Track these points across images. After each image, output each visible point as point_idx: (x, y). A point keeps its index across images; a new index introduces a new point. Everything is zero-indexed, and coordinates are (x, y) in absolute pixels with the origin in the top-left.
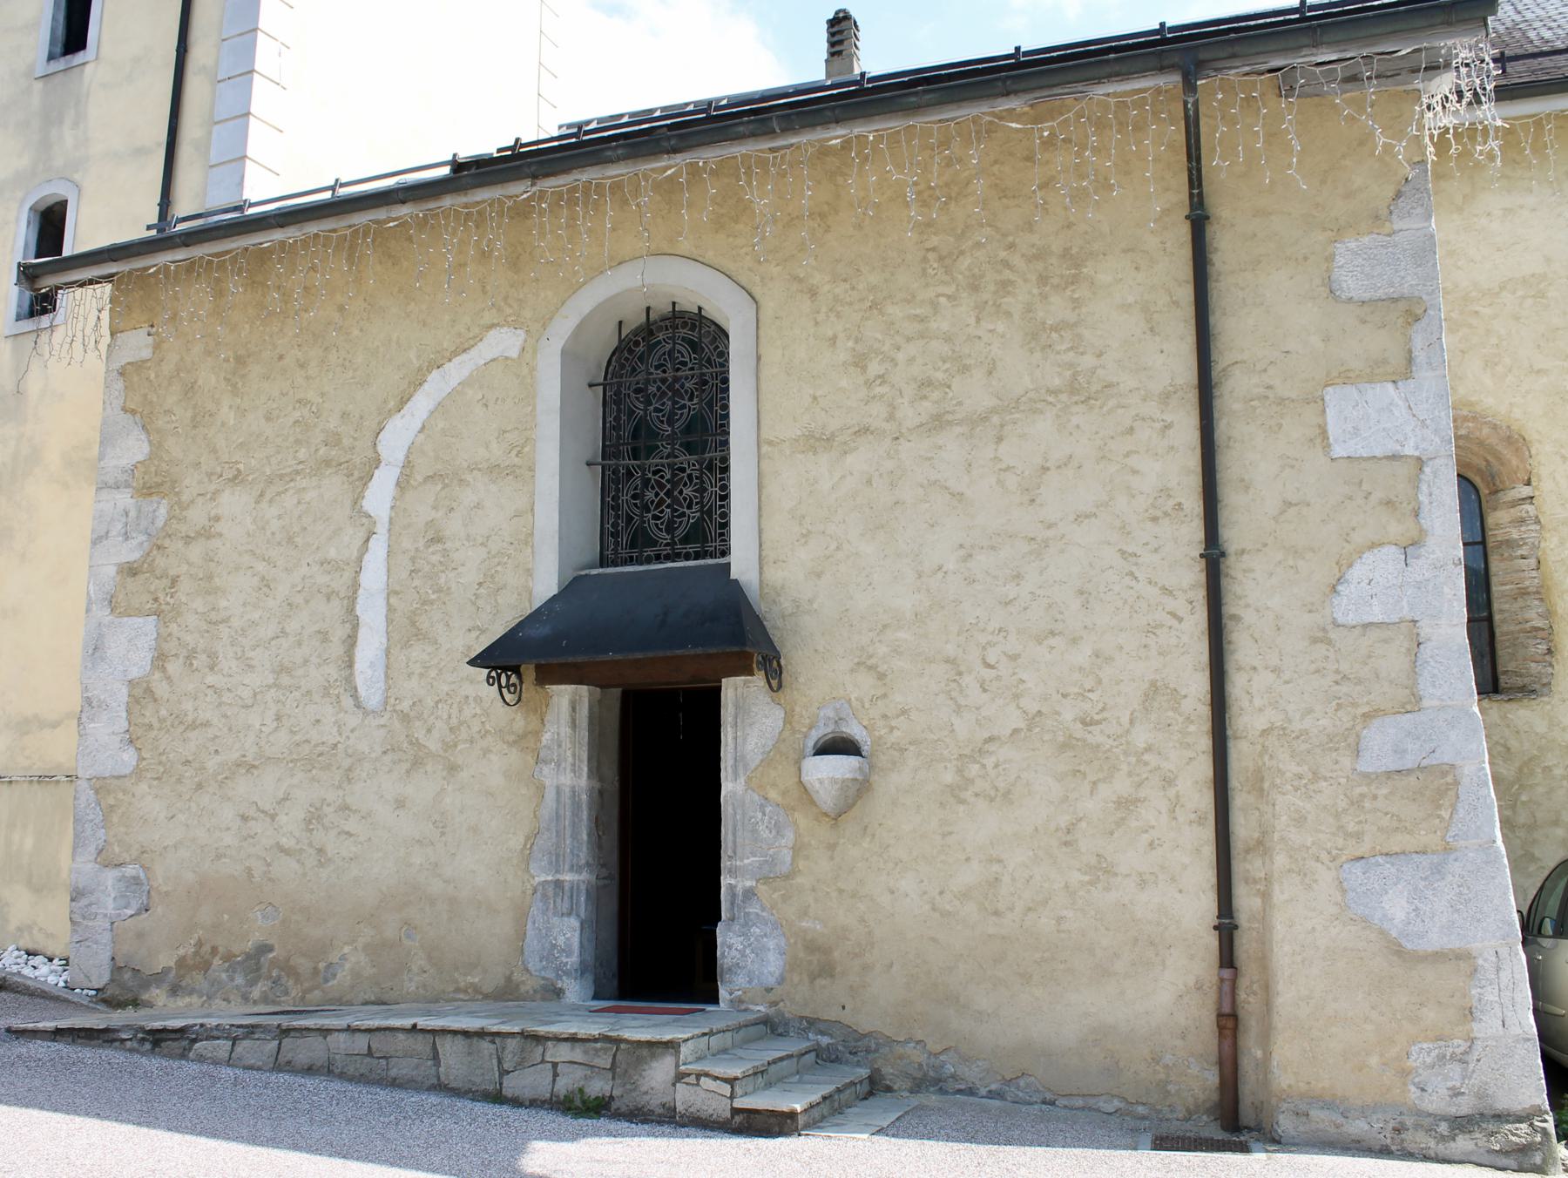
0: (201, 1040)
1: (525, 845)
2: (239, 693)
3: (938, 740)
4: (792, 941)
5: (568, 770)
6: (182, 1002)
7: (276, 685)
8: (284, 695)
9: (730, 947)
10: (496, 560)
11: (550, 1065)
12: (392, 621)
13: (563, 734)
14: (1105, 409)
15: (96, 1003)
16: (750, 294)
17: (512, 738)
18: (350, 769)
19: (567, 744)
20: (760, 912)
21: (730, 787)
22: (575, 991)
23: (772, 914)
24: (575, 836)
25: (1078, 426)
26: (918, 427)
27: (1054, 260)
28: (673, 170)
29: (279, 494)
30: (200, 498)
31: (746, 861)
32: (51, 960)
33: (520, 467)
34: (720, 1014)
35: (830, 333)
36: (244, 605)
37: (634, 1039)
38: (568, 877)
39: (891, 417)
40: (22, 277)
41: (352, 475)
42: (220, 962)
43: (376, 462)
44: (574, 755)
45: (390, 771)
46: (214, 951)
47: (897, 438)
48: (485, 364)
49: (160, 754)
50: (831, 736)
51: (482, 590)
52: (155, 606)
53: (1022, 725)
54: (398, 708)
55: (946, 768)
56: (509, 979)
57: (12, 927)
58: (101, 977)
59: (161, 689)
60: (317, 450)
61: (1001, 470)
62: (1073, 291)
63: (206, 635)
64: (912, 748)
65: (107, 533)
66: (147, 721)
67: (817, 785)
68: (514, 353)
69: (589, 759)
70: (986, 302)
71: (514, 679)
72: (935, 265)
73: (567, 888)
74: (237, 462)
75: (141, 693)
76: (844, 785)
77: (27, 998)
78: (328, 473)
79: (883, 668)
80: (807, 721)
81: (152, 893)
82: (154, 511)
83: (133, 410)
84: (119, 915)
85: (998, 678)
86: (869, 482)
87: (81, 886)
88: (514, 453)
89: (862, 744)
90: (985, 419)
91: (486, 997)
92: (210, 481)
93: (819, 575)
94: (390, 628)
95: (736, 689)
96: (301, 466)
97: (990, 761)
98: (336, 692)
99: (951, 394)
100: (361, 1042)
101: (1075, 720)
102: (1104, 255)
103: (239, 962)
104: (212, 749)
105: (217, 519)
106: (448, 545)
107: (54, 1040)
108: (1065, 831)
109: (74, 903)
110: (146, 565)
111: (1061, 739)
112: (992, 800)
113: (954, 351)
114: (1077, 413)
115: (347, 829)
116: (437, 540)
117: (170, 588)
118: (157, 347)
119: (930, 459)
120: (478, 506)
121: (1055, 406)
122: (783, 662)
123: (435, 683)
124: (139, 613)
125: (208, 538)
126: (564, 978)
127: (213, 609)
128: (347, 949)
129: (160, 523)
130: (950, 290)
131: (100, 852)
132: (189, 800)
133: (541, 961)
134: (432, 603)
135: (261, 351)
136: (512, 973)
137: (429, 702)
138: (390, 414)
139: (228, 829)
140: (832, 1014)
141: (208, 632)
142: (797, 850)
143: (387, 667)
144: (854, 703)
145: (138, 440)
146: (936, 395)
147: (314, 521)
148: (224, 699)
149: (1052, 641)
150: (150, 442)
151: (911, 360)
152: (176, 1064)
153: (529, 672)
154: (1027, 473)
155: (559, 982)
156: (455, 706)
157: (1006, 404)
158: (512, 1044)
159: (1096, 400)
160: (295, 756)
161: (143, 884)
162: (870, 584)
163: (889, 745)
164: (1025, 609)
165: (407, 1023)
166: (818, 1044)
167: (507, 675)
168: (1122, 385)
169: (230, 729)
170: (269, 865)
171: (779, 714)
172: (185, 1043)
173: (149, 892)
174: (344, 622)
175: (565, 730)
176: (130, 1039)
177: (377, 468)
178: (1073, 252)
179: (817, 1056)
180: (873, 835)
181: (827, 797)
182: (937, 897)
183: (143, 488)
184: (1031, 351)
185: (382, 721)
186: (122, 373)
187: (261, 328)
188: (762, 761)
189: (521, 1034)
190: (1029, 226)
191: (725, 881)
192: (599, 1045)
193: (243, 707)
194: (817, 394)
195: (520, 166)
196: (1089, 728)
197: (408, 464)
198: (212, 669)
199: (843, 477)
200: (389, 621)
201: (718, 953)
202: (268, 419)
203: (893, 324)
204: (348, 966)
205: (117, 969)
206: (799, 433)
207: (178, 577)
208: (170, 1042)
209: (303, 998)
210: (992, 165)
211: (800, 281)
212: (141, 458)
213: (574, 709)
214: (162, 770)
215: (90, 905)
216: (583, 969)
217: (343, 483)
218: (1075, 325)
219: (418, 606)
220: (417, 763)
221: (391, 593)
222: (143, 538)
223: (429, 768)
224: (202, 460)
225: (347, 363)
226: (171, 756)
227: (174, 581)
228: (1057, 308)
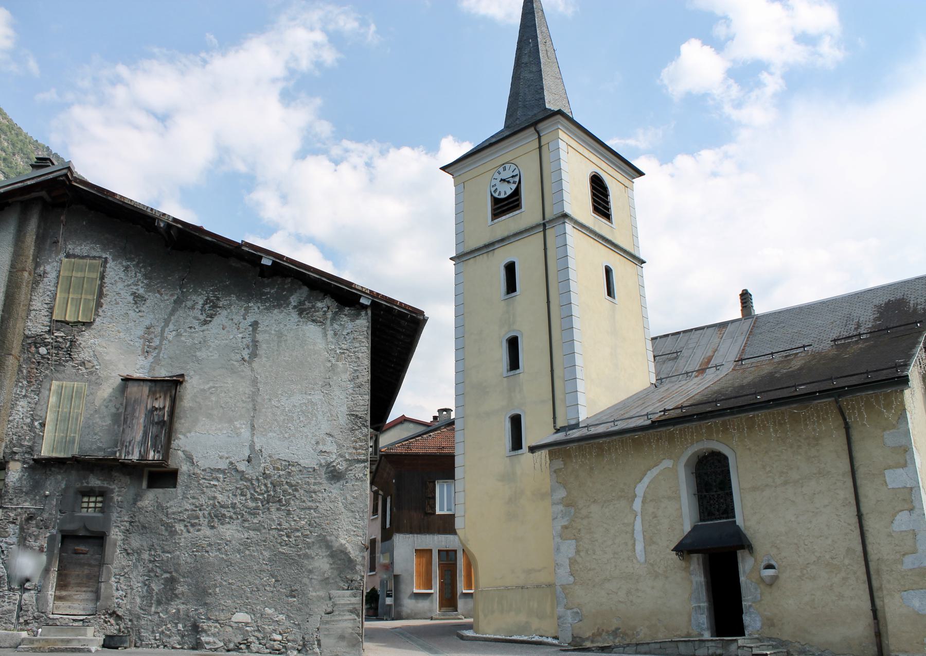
21: (742, 579)
43: (635, 496)
53: (816, 559)
59: (579, 559)
68: (671, 466)
79: (778, 546)
93: (760, 523)
105: (590, 513)
116: (655, 517)
120: (666, 508)
124: (570, 539)
130: (785, 448)
137: (658, 560)
143: (645, 551)
158: (696, 643)
169: (601, 570)
197: (644, 497)
198: (594, 554)
200: (644, 539)
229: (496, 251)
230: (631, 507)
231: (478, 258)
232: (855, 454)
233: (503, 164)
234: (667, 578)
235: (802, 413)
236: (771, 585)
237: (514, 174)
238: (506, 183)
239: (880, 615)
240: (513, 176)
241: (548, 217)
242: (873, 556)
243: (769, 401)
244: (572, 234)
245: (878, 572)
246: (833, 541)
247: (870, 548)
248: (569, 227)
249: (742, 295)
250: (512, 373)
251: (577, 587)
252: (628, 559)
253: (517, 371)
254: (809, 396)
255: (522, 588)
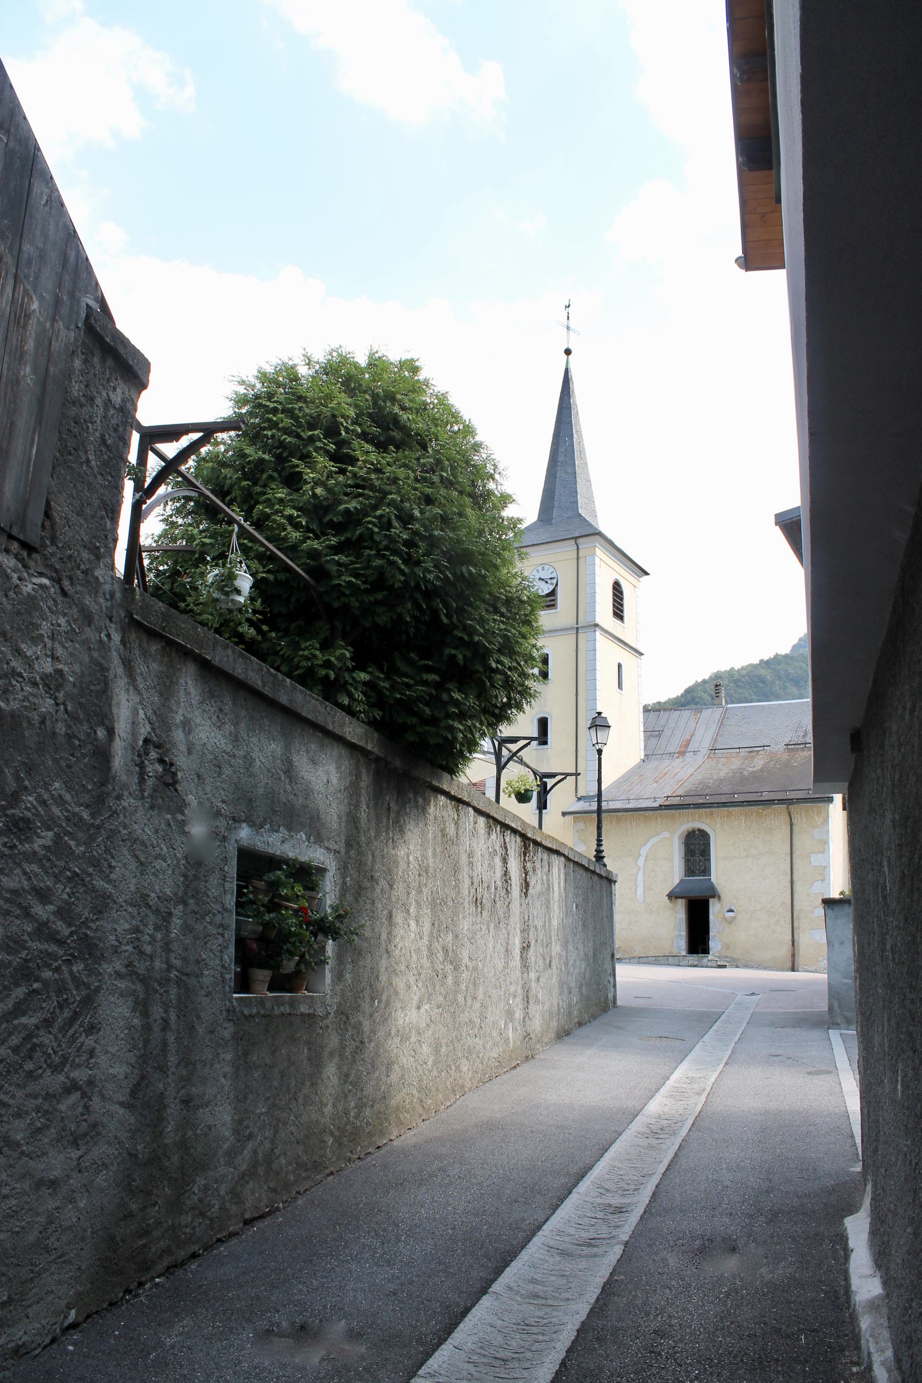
21: (711, 917)
43: (640, 855)
116: (654, 871)
197: (647, 856)
230: (636, 862)
232: (794, 842)
234: (658, 914)
236: (730, 923)
237: (552, 576)
238: (544, 582)
239: (796, 944)
240: (551, 579)
241: (580, 625)
242: (796, 908)
243: (744, 802)
244: (600, 639)
245: (798, 918)
247: (795, 903)
253: (546, 747)
254: (771, 802)
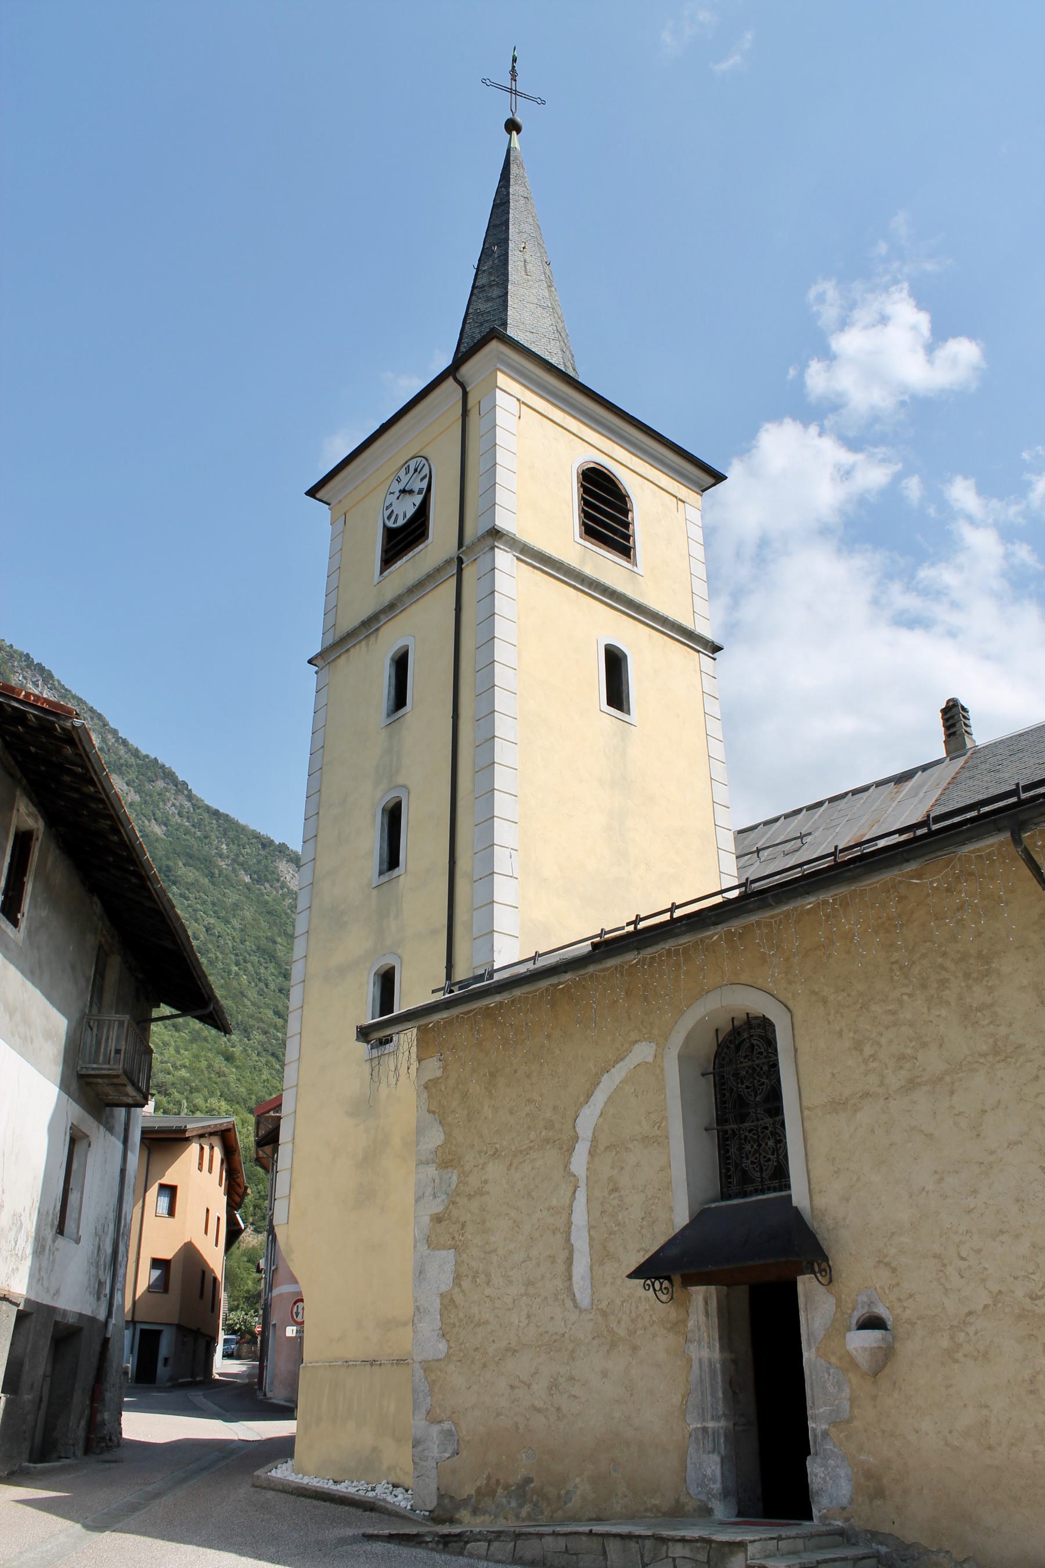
0: (471, 1542)
1: (682, 1401)
2: (505, 1300)
3: (936, 1316)
4: (855, 1470)
5: (705, 1347)
6: (479, 1519)
7: (526, 1294)
8: (531, 1300)
9: (816, 1475)
10: (651, 1202)
11: (671, 1559)
12: (592, 1247)
13: (701, 1321)
14: (1018, 1064)
15: (427, 1520)
16: (786, 1006)
17: (669, 1325)
18: (573, 1351)
19: (703, 1328)
20: (832, 1448)
21: (808, 1355)
22: (720, 1510)
23: (841, 1450)
24: (713, 1394)
25: (1002, 1079)
26: (899, 1089)
27: (972, 961)
28: (811, 905)
29: (521, 1163)
30: (475, 1168)
31: (821, 1410)
32: (407, 1491)
33: (660, 1137)
34: (806, 1526)
35: (838, 1029)
36: (505, 1240)
37: (719, 1540)
38: (711, 1424)
39: (882, 1084)
40: (359, 1035)
41: (562, 1148)
42: (502, 1491)
43: (576, 1138)
44: (709, 1336)
45: (598, 1351)
46: (498, 1482)
47: (887, 1098)
48: (634, 1068)
49: (460, 1344)
50: (867, 1315)
51: (644, 1223)
52: (453, 1242)
53: (989, 1301)
54: (599, 1307)
55: (942, 1336)
56: (677, 1501)
57: (384, 1468)
58: (432, 1503)
59: (459, 1299)
60: (540, 1133)
61: (955, 1115)
62: (988, 981)
63: (483, 1261)
64: (919, 1322)
65: (424, 1194)
66: (452, 1321)
67: (855, 1353)
68: (650, 1059)
69: (720, 1338)
70: (933, 996)
71: (666, 1283)
72: (898, 973)
73: (710, 1433)
74: (495, 1143)
75: (448, 1303)
76: (873, 1352)
77: (386, 1517)
78: (548, 1147)
79: (894, 1264)
80: (850, 1305)
81: (460, 1441)
82: (450, 1178)
83: (434, 1111)
84: (441, 1457)
85: (970, 1267)
86: (873, 1131)
87: (418, 1437)
88: (656, 1127)
89: (887, 1320)
90: (941, 1079)
91: (664, 1514)
92: (480, 1156)
93: (848, 1200)
94: (592, 1251)
95: (805, 1284)
96: (532, 1144)
97: (971, 1330)
98: (562, 1297)
99: (918, 1064)
100: (561, 1543)
101: (1024, 1296)
102: (1005, 952)
103: (513, 1491)
104: (491, 1339)
105: (486, 1182)
106: (622, 1193)
107: (389, 1542)
108: (1029, 1382)
109: (414, 1449)
110: (446, 1215)
111: (1017, 1311)
112: (976, 1360)
113: (916, 1033)
114: (1001, 1069)
115: (573, 1393)
116: (615, 1190)
117: (461, 1230)
118: (445, 1068)
119: (909, 1111)
120: (638, 1165)
121: (985, 1065)
122: (831, 1263)
123: (620, 1289)
124: (444, 1247)
125: (482, 1195)
126: (713, 1500)
127: (487, 1243)
128: (578, 1480)
129: (453, 1186)
130: (909, 990)
131: (428, 1413)
132: (479, 1375)
133: (697, 1487)
134: (614, 1233)
135: (503, 1068)
136: (680, 1496)
137: (618, 1302)
138: (582, 1105)
139: (503, 1395)
140: (886, 1528)
141: (484, 1259)
142: (852, 1400)
143: (592, 1279)
144: (879, 1290)
145: (438, 1131)
146: (908, 1065)
147: (542, 1181)
148: (497, 1305)
149: (1004, 1238)
150: (444, 1132)
151: (890, 1042)
152: (454, 1558)
153: (677, 1279)
154: (972, 1115)
155: (710, 1503)
156: (633, 1304)
157: (953, 1067)
158: (648, 1543)
159: (1011, 1058)
160: (540, 1343)
161: (454, 1435)
162: (880, 1204)
163: (904, 1321)
164: (982, 1215)
165: (586, 1529)
166: (878, 1551)
167: (660, 1282)
168: (1027, 1045)
169: (501, 1326)
170: (528, 1420)
171: (832, 1300)
172: (462, 1544)
173: (458, 1441)
174: (564, 1249)
175: (702, 1318)
176: (431, 1542)
177: (577, 1142)
178: (984, 953)
179: (879, 1562)
180: (900, 1389)
181: (864, 1361)
182: (948, 1436)
183: (442, 1163)
184: (966, 1027)
185: (591, 1316)
186: (426, 1087)
187: (503, 1052)
188: (825, 1335)
189: (652, 1536)
190: (954, 939)
191: (811, 1424)
192: (699, 1544)
193: (507, 1310)
194: (835, 1072)
195: (796, 888)
196: (1036, 1302)
197: (594, 1140)
198: (488, 1284)
199: (857, 1128)
200: (591, 1247)
201: (809, 1480)
202: (511, 1113)
203: (876, 1018)
204: (578, 1493)
205: (441, 1497)
206: (826, 1100)
207: (465, 1222)
208: (453, 1544)
209: (552, 1517)
210: (926, 898)
211: (816, 994)
212: (440, 1143)
213: (706, 1303)
214: (462, 1354)
215: (424, 1450)
216: (725, 1494)
217: (557, 1154)
218: (992, 1005)
219: (607, 1236)
220: (613, 1345)
221: (591, 1227)
222: (444, 1197)
223: (620, 1348)
224: (475, 1143)
225: (554, 1073)
226: (467, 1345)
227: (463, 1226)
228: (978, 995)
229: (381, 632)
231: (352, 650)
233: (406, 463)
235: (932, 882)
246: (1034, 1246)
248: (504, 559)
249: (945, 711)
250: (385, 878)
251: (452, 1367)
252: (556, 1299)
255: (372, 1365)
